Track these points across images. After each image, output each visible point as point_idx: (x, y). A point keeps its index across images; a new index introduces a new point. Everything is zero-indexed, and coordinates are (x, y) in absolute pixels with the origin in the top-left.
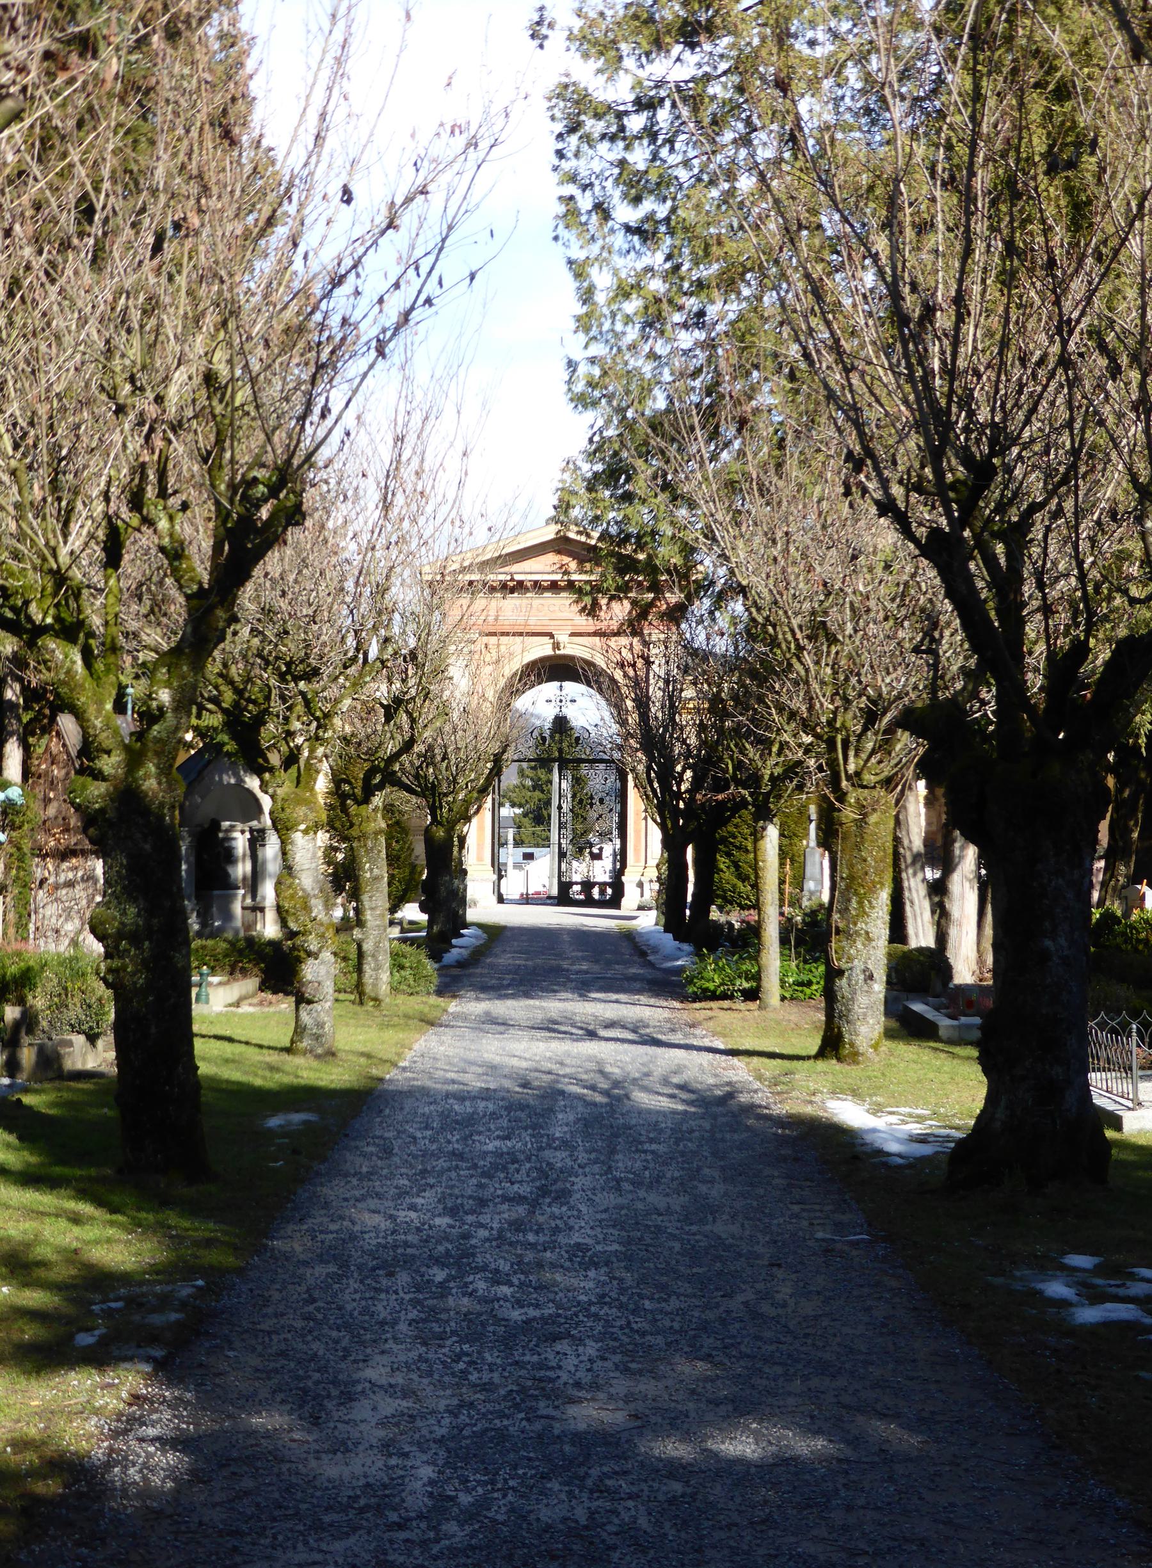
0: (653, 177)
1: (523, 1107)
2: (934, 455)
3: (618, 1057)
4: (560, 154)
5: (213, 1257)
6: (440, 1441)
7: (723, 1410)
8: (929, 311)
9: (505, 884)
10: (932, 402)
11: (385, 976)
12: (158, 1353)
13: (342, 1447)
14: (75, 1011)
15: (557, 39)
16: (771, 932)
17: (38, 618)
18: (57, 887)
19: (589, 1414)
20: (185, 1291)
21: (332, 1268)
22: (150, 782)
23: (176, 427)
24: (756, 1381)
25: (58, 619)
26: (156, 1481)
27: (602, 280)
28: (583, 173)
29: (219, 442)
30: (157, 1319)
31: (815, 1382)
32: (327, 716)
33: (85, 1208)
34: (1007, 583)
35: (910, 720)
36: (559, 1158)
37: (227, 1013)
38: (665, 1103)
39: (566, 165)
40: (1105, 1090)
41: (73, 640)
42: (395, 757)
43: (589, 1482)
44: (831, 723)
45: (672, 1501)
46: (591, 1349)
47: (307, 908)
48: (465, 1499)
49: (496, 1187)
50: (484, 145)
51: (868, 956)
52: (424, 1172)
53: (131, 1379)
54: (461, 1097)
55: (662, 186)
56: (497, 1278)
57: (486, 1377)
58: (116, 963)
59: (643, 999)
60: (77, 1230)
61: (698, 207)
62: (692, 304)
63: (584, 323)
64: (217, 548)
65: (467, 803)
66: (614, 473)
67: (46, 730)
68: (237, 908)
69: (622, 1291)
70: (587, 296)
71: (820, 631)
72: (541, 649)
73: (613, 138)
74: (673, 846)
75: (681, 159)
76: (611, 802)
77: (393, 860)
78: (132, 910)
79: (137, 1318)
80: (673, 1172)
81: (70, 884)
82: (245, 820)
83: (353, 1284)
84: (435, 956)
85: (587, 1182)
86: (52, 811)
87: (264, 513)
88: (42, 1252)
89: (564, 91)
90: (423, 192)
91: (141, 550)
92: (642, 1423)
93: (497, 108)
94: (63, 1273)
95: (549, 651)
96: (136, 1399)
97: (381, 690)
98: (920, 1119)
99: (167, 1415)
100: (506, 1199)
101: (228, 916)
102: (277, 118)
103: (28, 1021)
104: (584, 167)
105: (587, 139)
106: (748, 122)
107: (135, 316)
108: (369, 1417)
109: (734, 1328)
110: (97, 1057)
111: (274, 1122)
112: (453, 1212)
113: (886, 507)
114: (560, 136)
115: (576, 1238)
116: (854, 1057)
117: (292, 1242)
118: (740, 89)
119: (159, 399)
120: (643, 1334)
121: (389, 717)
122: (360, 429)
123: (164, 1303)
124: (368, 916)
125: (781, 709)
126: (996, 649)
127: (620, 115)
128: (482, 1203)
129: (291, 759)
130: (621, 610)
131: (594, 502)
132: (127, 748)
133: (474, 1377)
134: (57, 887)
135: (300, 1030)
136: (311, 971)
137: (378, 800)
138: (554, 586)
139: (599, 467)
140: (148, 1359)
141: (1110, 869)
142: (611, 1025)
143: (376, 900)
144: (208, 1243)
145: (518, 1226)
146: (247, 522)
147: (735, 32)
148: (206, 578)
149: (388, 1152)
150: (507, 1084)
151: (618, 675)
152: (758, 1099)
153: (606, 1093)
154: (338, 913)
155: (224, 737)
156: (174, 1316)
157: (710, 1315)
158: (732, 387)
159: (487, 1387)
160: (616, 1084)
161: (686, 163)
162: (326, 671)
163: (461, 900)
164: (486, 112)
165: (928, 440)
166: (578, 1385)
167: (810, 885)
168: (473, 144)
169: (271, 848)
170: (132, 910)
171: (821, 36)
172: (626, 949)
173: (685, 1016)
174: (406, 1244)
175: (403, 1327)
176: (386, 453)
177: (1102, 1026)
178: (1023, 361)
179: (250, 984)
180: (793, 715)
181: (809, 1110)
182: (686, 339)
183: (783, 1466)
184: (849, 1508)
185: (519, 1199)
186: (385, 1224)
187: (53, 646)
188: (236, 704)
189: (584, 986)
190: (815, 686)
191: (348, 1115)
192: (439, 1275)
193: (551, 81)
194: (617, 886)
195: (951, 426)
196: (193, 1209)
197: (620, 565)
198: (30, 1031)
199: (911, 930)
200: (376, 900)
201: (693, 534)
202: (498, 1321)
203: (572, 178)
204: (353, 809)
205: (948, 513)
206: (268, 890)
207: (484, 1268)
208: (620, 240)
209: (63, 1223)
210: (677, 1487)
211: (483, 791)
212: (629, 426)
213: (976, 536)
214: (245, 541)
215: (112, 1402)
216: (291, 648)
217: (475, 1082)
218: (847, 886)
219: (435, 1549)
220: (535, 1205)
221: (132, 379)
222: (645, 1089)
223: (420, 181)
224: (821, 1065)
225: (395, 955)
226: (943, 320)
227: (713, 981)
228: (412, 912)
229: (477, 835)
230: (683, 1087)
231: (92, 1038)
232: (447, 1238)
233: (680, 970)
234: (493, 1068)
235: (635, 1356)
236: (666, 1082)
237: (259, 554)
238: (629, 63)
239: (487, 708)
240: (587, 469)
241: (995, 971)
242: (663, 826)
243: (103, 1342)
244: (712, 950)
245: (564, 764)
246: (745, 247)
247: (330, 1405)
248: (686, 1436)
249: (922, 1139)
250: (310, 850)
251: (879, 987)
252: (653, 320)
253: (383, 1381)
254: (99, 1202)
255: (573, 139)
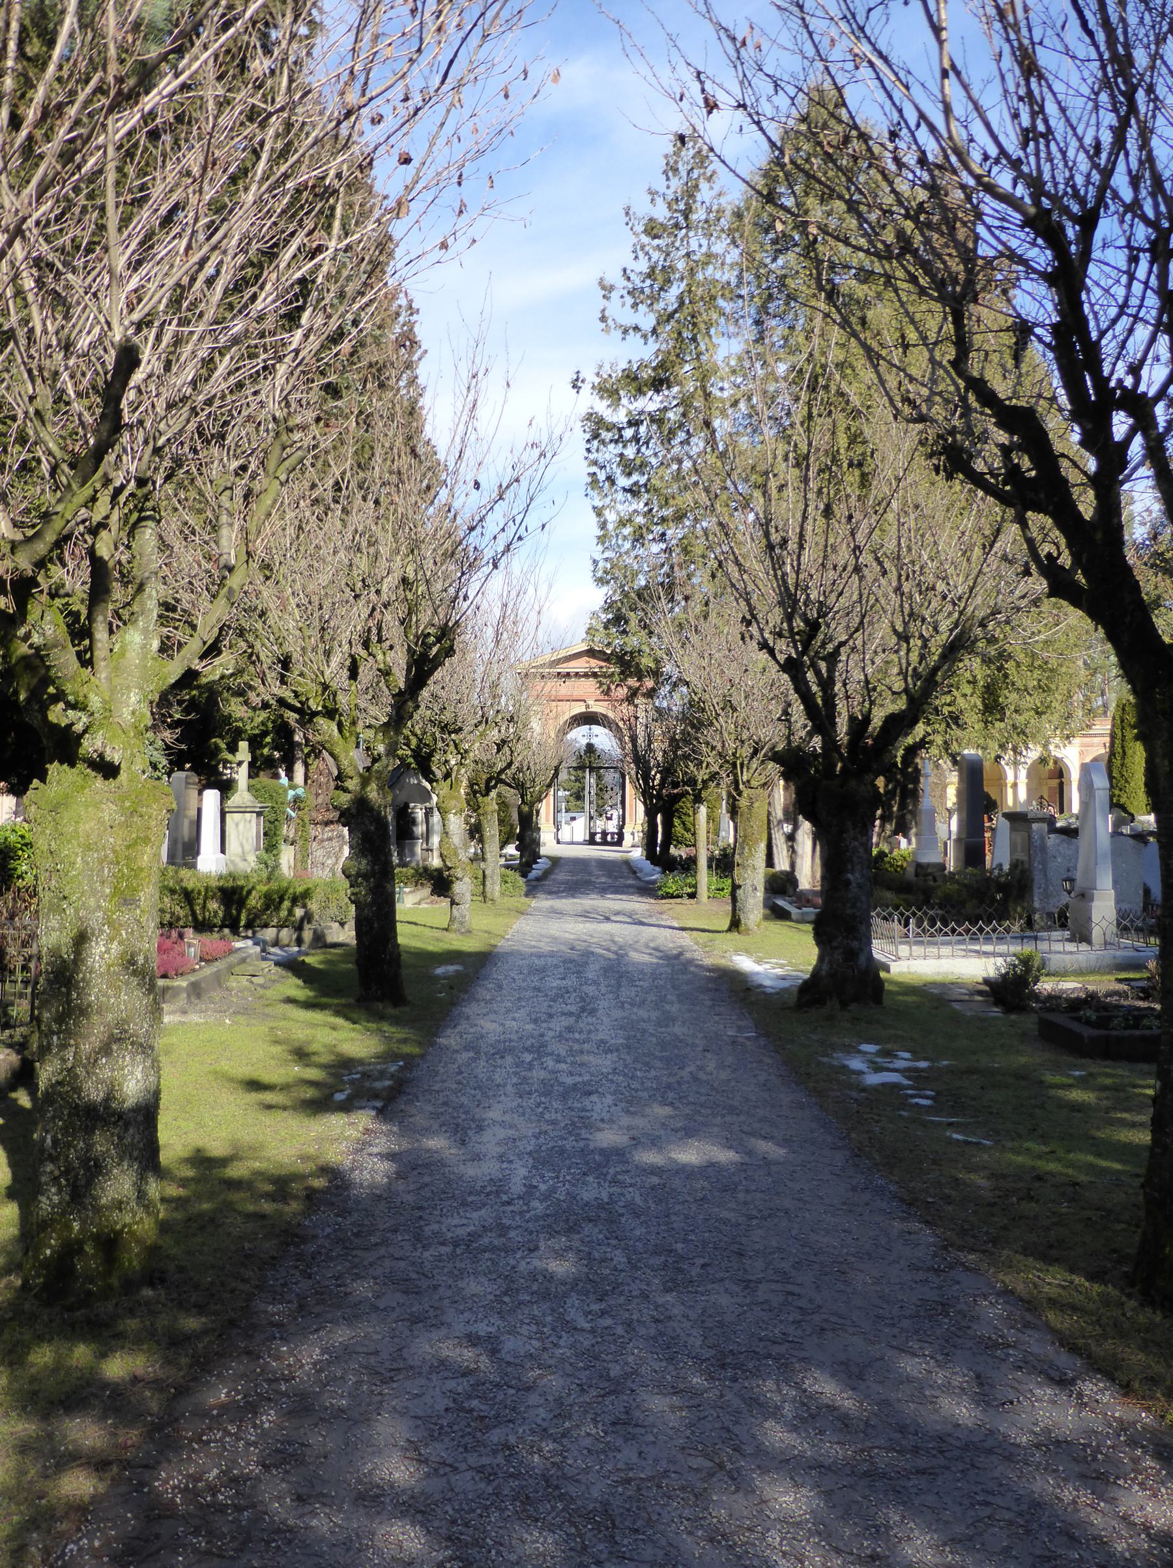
0: (638, 462)
1: (571, 961)
2: (789, 618)
3: (621, 932)
4: (588, 450)
5: (407, 1049)
6: (530, 1154)
7: (679, 1134)
8: (785, 541)
9: (563, 834)
10: (787, 589)
11: (497, 888)
12: (379, 1104)
13: (477, 1158)
14: (333, 910)
15: (586, 389)
16: (703, 862)
17: (314, 707)
18: (322, 841)
19: (608, 1138)
20: (393, 1069)
21: (471, 1054)
22: (373, 793)
23: (386, 606)
24: (697, 1117)
25: (324, 707)
26: (378, 1178)
27: (611, 517)
28: (601, 460)
29: (410, 614)
30: (378, 1085)
31: (728, 1119)
32: (466, 751)
33: (339, 1021)
34: (827, 684)
35: (776, 757)
36: (591, 990)
37: (412, 905)
38: (646, 958)
39: (592, 457)
40: (880, 950)
41: (333, 719)
42: (502, 771)
43: (609, 1177)
44: (734, 754)
45: (653, 1188)
46: (609, 1099)
47: (456, 854)
48: (543, 1187)
49: (558, 1007)
50: (549, 455)
51: (753, 877)
52: (519, 999)
53: (363, 1119)
54: (539, 956)
55: (643, 466)
56: (559, 1060)
57: (554, 1116)
58: (356, 890)
59: (634, 898)
60: (335, 1034)
61: (662, 478)
62: (658, 529)
63: (601, 540)
64: (409, 670)
65: (541, 792)
66: (618, 620)
67: (317, 757)
68: (418, 850)
69: (626, 1066)
70: (603, 525)
71: (730, 706)
72: (579, 708)
73: (616, 442)
74: (650, 814)
75: (652, 453)
76: (617, 789)
77: (501, 822)
78: (364, 862)
79: (367, 1084)
80: (651, 997)
81: (330, 839)
82: (423, 802)
83: (483, 1063)
84: (524, 875)
85: (606, 1004)
86: (320, 800)
87: (435, 650)
88: (314, 1047)
89: (589, 417)
90: (517, 480)
91: (366, 673)
92: (636, 1142)
93: (556, 435)
94: (325, 1059)
95: (583, 710)
96: (367, 1131)
97: (494, 735)
98: (782, 966)
99: (384, 1140)
100: (563, 1014)
101: (413, 854)
102: (439, 426)
103: (308, 917)
104: (600, 457)
105: (603, 442)
106: (688, 432)
107: (364, 544)
108: (490, 1141)
109: (685, 1087)
110: (346, 935)
111: (440, 971)
112: (535, 1021)
113: (764, 645)
114: (588, 441)
115: (600, 1036)
116: (748, 931)
117: (450, 1039)
118: (684, 415)
119: (378, 592)
120: (637, 1091)
121: (499, 750)
122: (486, 594)
123: (382, 1075)
124: (488, 856)
125: (707, 743)
126: (821, 718)
127: (620, 429)
128: (551, 1016)
129: (447, 776)
130: (622, 692)
131: (608, 635)
132: (361, 776)
133: (547, 1116)
134: (322, 841)
135: (452, 919)
136: (458, 888)
137: (493, 794)
138: (586, 675)
139: (610, 616)
140: (374, 1108)
141: (882, 826)
142: (617, 913)
143: (492, 846)
144: (405, 1041)
145: (570, 1029)
146: (424, 656)
147: (680, 384)
148: (402, 685)
149: (500, 987)
150: (563, 948)
151: (621, 724)
152: (697, 955)
153: (615, 953)
154: (472, 850)
155: (411, 760)
156: (388, 1083)
157: (672, 1080)
158: (679, 574)
159: (554, 1122)
160: (621, 948)
161: (656, 454)
162: (467, 729)
163: (537, 843)
164: (550, 438)
165: (785, 610)
166: (602, 1120)
167: (723, 834)
168: (543, 455)
169: (436, 818)
170: (364, 862)
171: (726, 386)
172: (625, 869)
173: (657, 908)
174: (511, 1041)
175: (509, 1088)
176: (497, 612)
177: (878, 915)
178: (835, 568)
179: (427, 891)
180: (713, 748)
181: (723, 962)
182: (656, 548)
183: (710, 1169)
184: (747, 1191)
185: (571, 1014)
186: (500, 1029)
187: (321, 721)
188: (418, 746)
189: (603, 891)
190: (725, 735)
191: (477, 966)
192: (528, 1057)
193: (583, 411)
194: (621, 835)
195: (796, 601)
196: (396, 1021)
197: (623, 666)
198: (309, 922)
199: (776, 861)
200: (492, 846)
201: (660, 653)
202: (561, 1084)
203: (595, 463)
204: (480, 799)
205: (796, 647)
206: (435, 840)
207: (552, 1054)
208: (620, 496)
209: (327, 1030)
210: (655, 1180)
211: (549, 786)
212: (626, 595)
213: (811, 660)
214: (422, 667)
215: (353, 1133)
216: (447, 717)
217: (545, 947)
218: (743, 839)
219: (528, 1216)
220: (578, 1017)
221: (363, 581)
222: (636, 950)
223: (515, 475)
224: (729, 935)
225: (503, 876)
226: (792, 546)
227: (672, 888)
228: (511, 850)
229: (545, 809)
230: (655, 949)
231: (342, 924)
232: (532, 1036)
233: (654, 882)
234: (555, 939)
235: (631, 1102)
236: (647, 946)
237: (431, 673)
238: (624, 401)
239: (551, 742)
240: (604, 617)
241: (823, 878)
242: (645, 803)
243: (350, 1099)
244: (671, 871)
245: (592, 769)
246: (687, 499)
247: (470, 1133)
248: (661, 1149)
249: (783, 978)
250: (457, 824)
251: (760, 894)
252: (639, 538)
253: (499, 1119)
254: (347, 1018)
255: (595, 443)
